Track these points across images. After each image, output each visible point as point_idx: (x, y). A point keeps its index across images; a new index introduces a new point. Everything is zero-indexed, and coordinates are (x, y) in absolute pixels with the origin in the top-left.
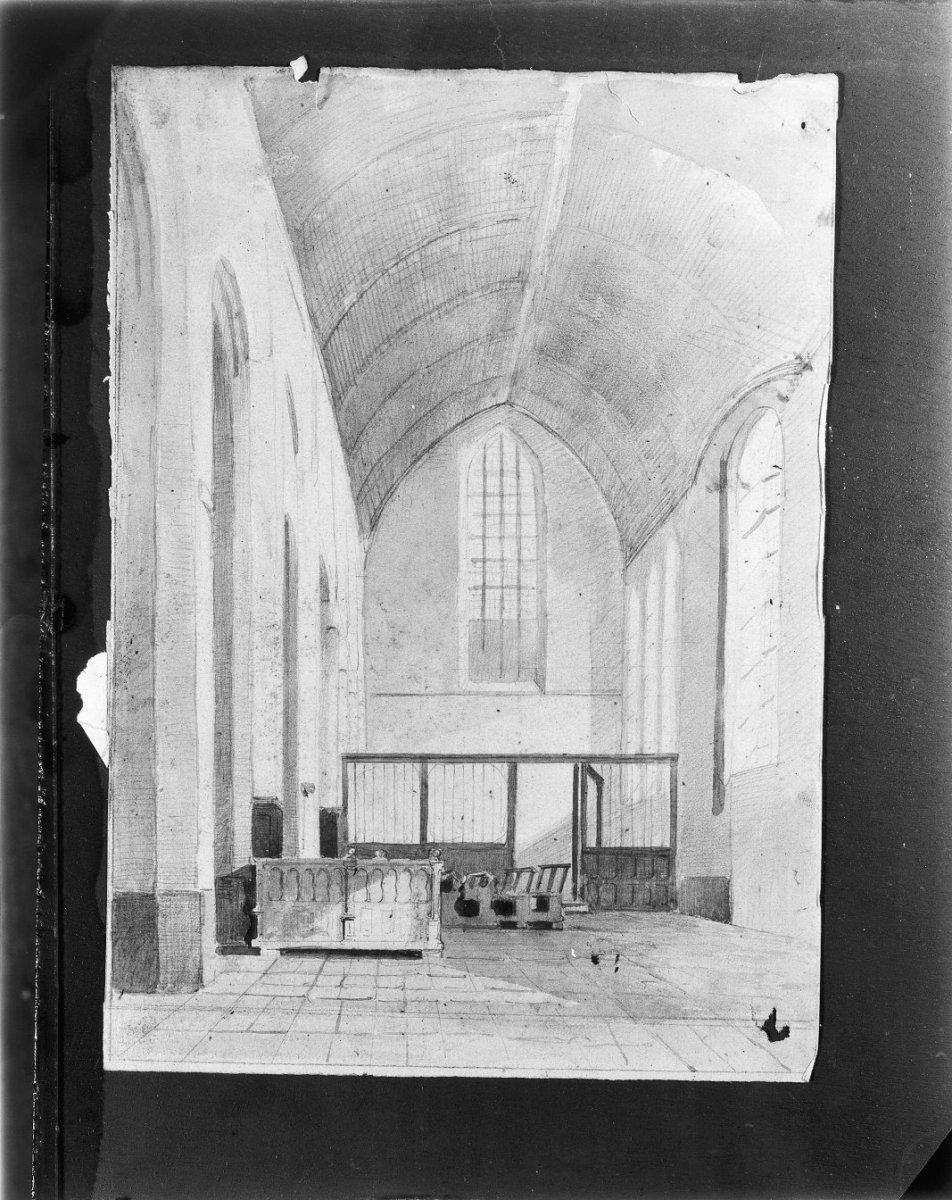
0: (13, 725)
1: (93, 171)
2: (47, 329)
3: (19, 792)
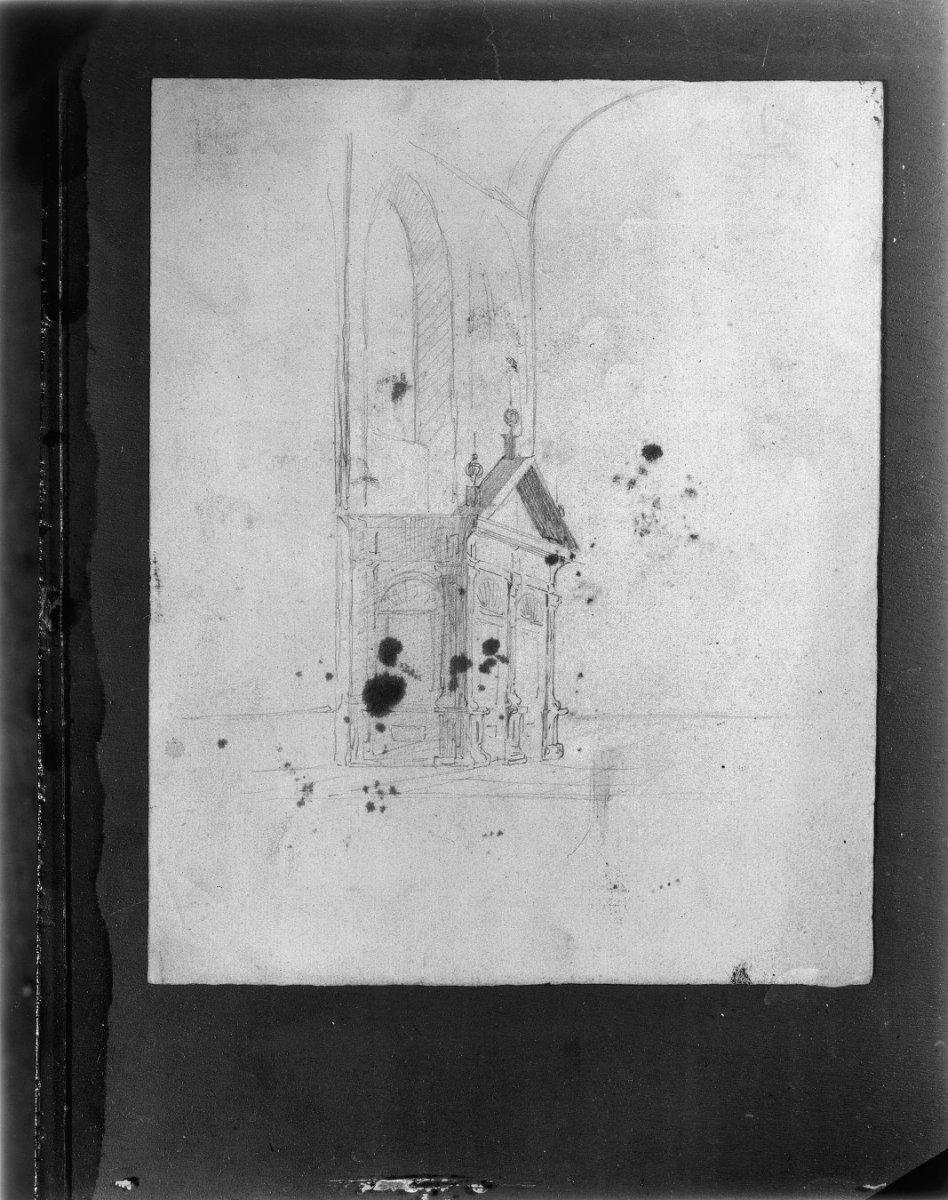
0: (12, 721)
1: (88, 168)
2: (43, 327)
3: (21, 789)
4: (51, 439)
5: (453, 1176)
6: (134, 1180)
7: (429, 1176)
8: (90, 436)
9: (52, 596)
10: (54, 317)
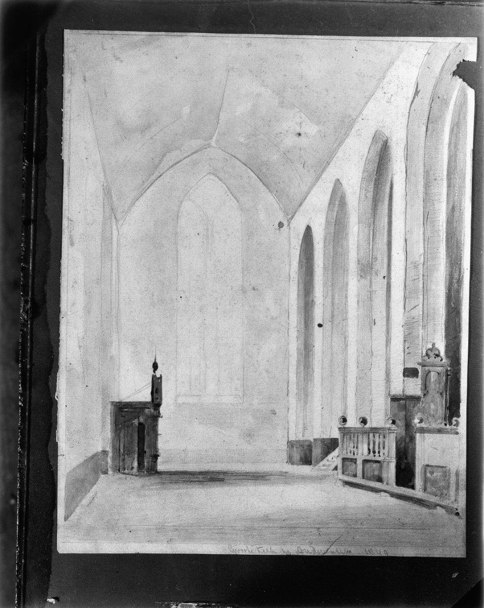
2: (24, 165)
4: (27, 223)
5: (218, 602)
6: (57, 599)
7: (206, 603)
8: (47, 220)
9: (26, 302)
10: (30, 161)
